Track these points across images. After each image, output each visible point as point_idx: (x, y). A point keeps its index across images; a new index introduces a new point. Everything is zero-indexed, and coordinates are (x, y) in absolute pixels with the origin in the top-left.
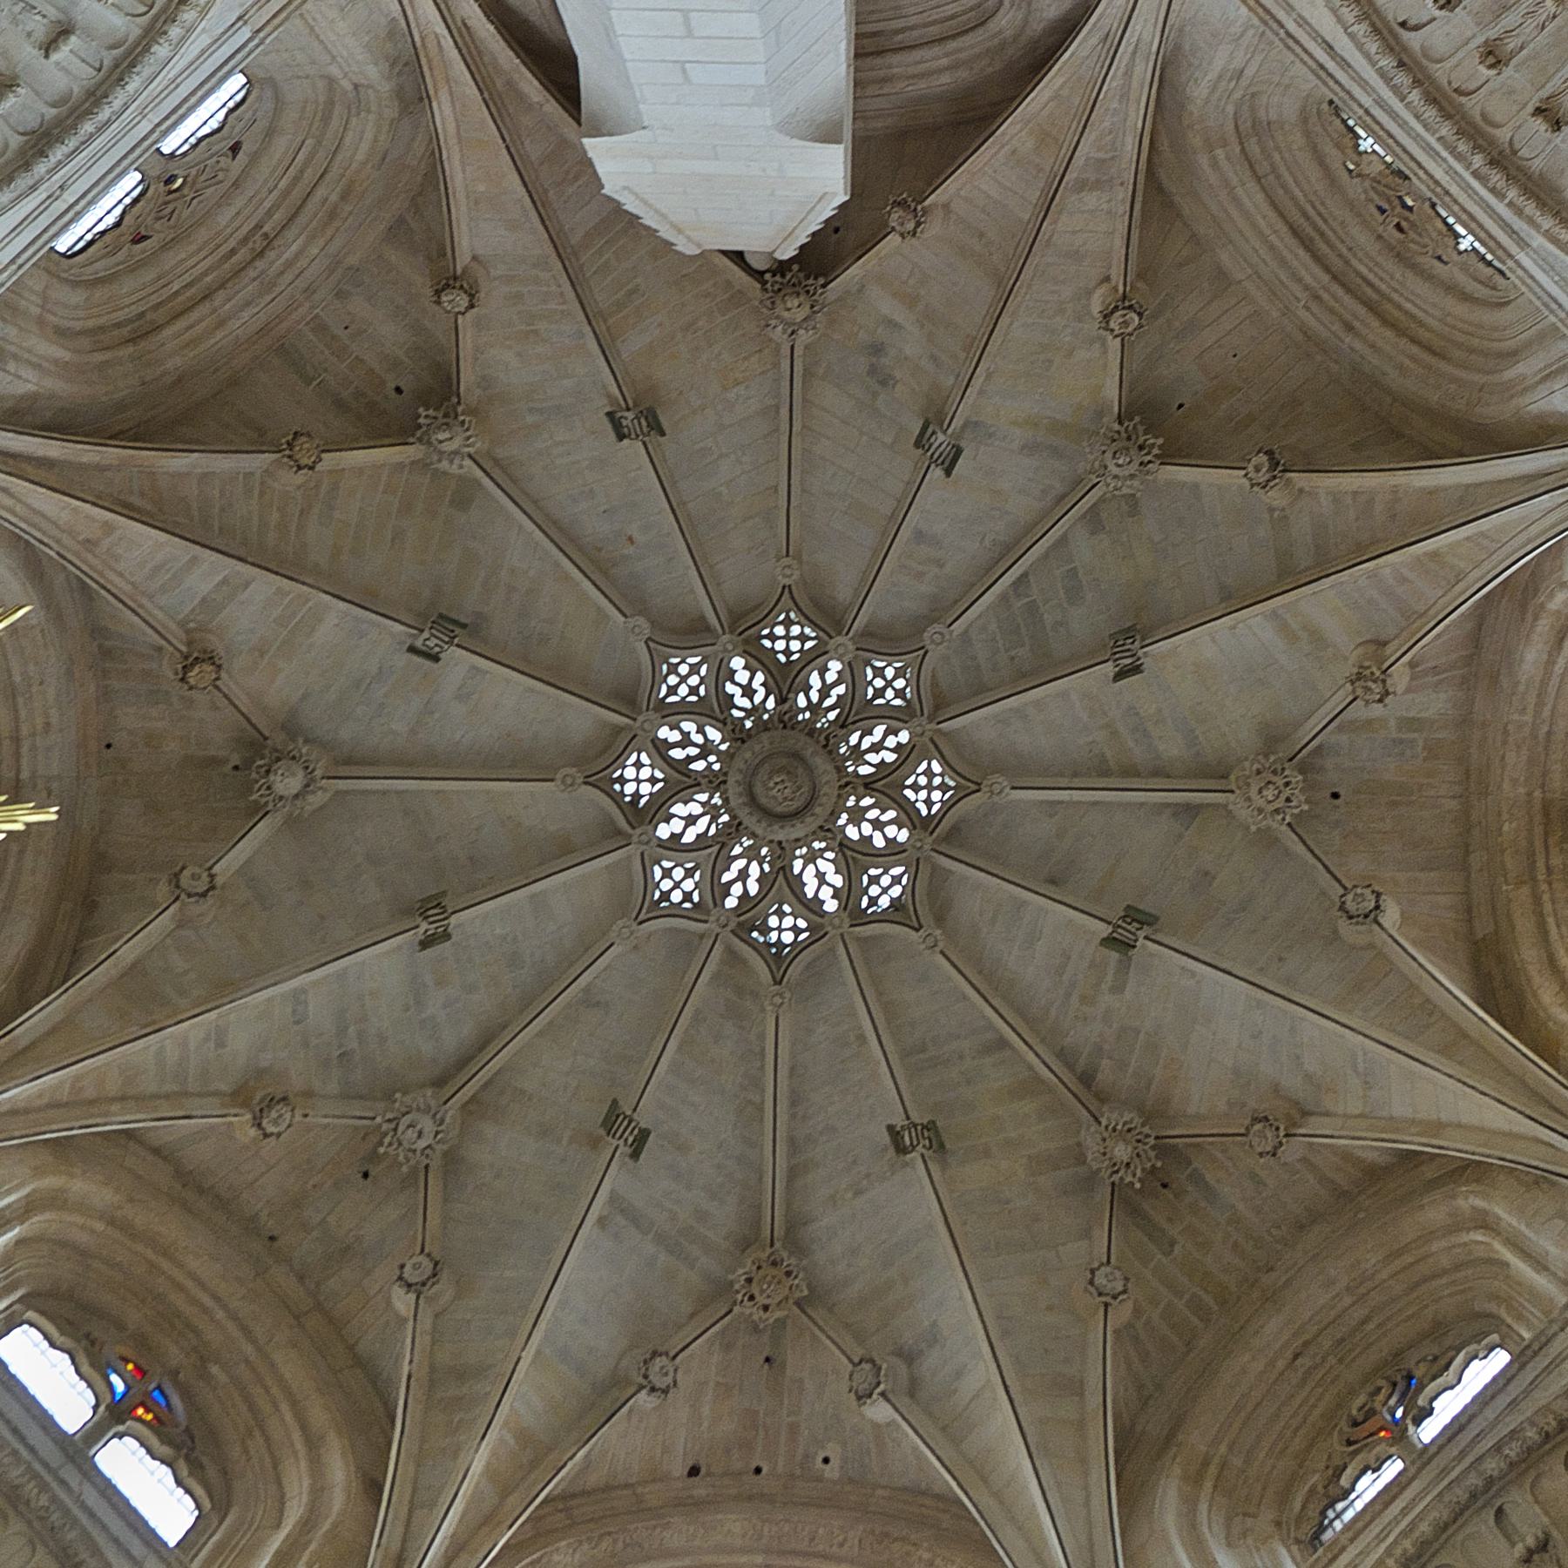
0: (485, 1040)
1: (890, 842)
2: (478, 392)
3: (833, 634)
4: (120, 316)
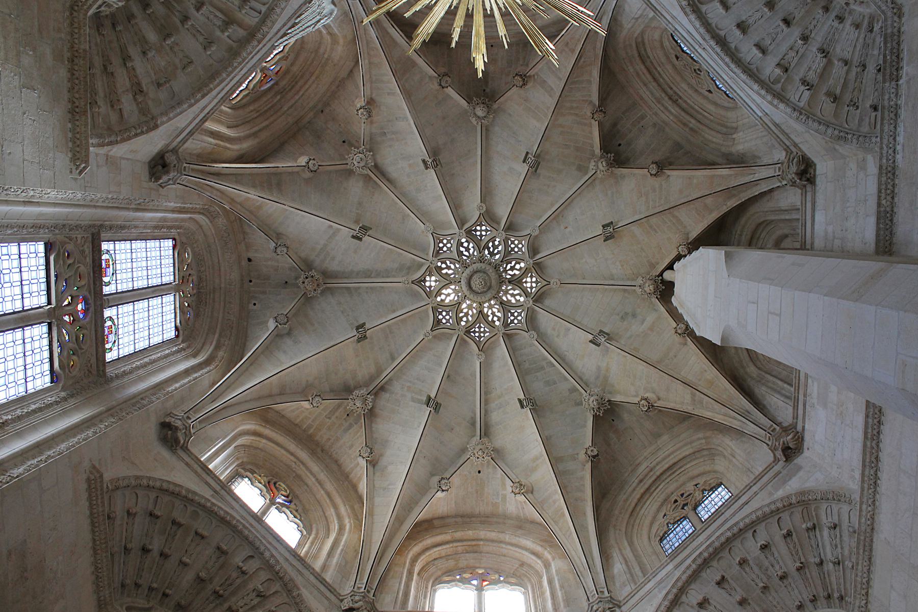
0: (390, 181)
4: (649, 50)
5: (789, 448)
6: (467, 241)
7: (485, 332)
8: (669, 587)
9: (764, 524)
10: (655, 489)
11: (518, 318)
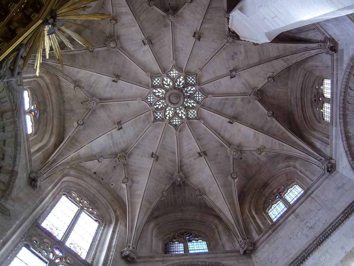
0: (110, 99)
1: (182, 116)
2: (180, 13)
3: (198, 85)
5: (332, 47)
6: (156, 90)
7: (194, 112)
8: (340, 136)
9: (350, 82)
10: (304, 103)
11: (199, 97)
